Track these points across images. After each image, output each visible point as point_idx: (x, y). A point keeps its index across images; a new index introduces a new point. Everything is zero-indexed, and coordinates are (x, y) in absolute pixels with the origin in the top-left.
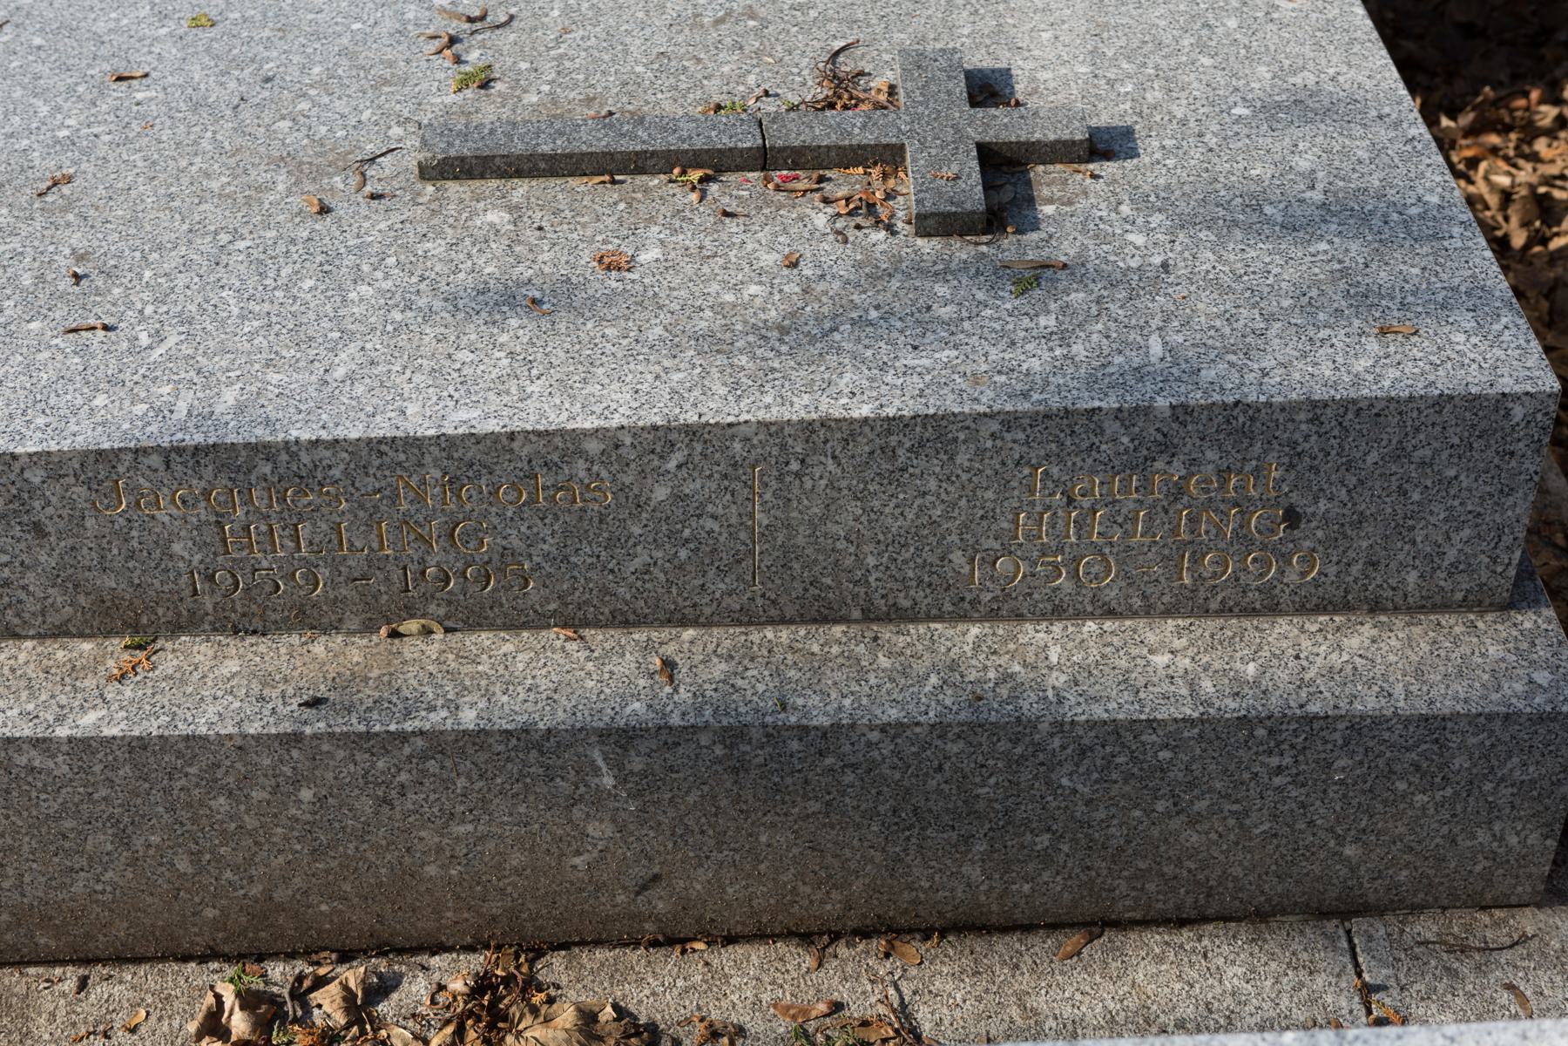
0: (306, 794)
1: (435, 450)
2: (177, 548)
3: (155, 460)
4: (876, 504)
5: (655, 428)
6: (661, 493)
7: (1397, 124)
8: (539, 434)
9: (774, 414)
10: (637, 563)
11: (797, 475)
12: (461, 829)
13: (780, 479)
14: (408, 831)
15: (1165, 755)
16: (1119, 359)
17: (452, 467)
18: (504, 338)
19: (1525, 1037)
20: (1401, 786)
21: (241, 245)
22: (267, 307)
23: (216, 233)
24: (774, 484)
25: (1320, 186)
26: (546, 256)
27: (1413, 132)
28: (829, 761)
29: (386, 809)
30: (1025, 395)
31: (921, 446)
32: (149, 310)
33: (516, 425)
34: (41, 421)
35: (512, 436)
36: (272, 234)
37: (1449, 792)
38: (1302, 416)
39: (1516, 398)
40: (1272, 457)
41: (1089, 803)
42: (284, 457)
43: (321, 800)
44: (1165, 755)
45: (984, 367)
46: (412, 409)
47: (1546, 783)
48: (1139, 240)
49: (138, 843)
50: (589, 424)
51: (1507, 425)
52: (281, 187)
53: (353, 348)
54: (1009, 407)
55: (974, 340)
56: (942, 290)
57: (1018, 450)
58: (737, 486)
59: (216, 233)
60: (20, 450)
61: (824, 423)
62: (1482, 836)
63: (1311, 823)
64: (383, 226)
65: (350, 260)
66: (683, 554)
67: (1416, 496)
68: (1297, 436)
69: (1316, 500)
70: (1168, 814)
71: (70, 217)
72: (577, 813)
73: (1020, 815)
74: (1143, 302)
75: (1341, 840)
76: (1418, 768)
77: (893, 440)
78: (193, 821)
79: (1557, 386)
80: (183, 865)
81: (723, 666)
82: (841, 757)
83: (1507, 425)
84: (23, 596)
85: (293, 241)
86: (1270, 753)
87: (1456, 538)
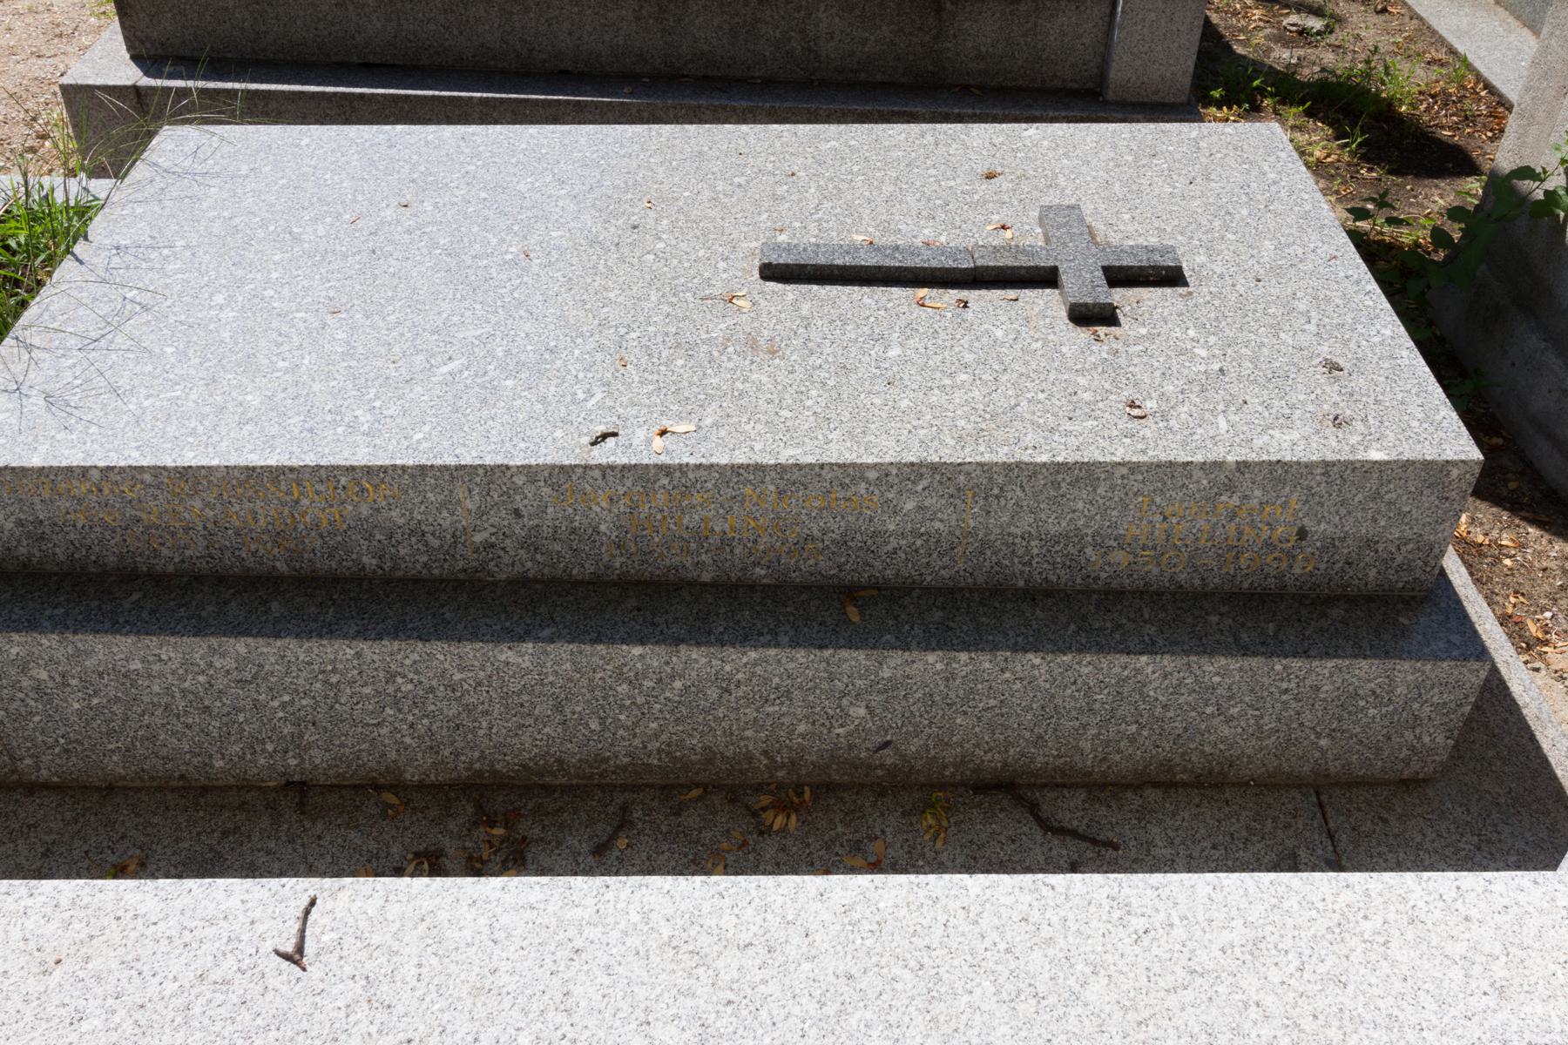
0: (678, 684)
1: (773, 474)
2: (603, 528)
3: (597, 474)
4: (1043, 516)
5: (912, 464)
6: (910, 505)
7: (1358, 282)
8: (839, 465)
9: (987, 458)
10: (890, 548)
11: (997, 497)
12: (770, 709)
13: (986, 498)
14: (738, 709)
15: (1217, 679)
16: (1200, 431)
17: (782, 484)
18: (809, 403)
19: (1536, 883)
20: (1362, 703)
21: (634, 335)
22: (656, 377)
23: (617, 327)
24: (982, 502)
25: (1314, 322)
26: (828, 350)
27: (1369, 287)
28: (1007, 675)
29: (726, 695)
30: (1144, 452)
31: (1077, 481)
32: (581, 375)
33: (825, 459)
34: (523, 445)
35: (822, 466)
36: (652, 329)
37: (1391, 708)
38: (1319, 471)
39: (1454, 463)
40: (1295, 496)
41: (1164, 706)
42: (678, 474)
43: (686, 688)
44: (1217, 679)
45: (1116, 433)
46: (758, 447)
47: (1453, 705)
48: (1204, 353)
49: (567, 710)
50: (871, 460)
51: (1447, 481)
52: (653, 298)
53: (714, 405)
54: (1134, 459)
55: (1107, 415)
56: (1082, 381)
57: (1136, 486)
58: (958, 502)
59: (617, 327)
60: (511, 463)
61: (1018, 465)
62: (1408, 735)
63: (1302, 724)
64: (723, 326)
65: (705, 348)
66: (919, 542)
67: (1383, 523)
68: (1313, 483)
69: (1319, 523)
70: (1213, 715)
71: (522, 312)
72: (845, 702)
73: (1120, 712)
74: (1210, 394)
75: (1319, 736)
76: (1374, 693)
77: (1060, 477)
78: (604, 698)
79: (1481, 457)
80: (594, 725)
81: (940, 614)
82: (1014, 673)
83: (1447, 481)
84: (502, 553)
85: (667, 334)
86: (1282, 680)
87: (1403, 549)
